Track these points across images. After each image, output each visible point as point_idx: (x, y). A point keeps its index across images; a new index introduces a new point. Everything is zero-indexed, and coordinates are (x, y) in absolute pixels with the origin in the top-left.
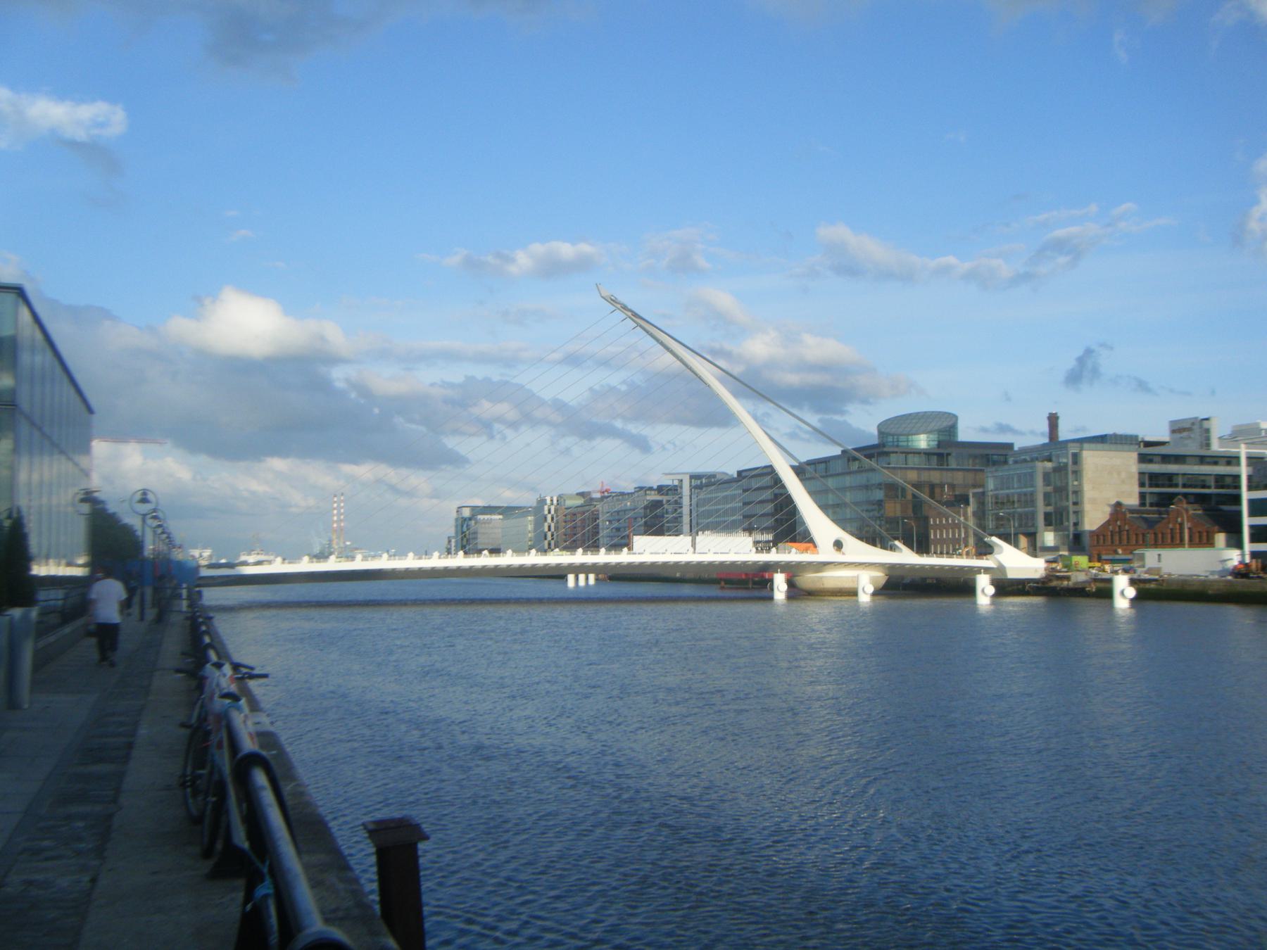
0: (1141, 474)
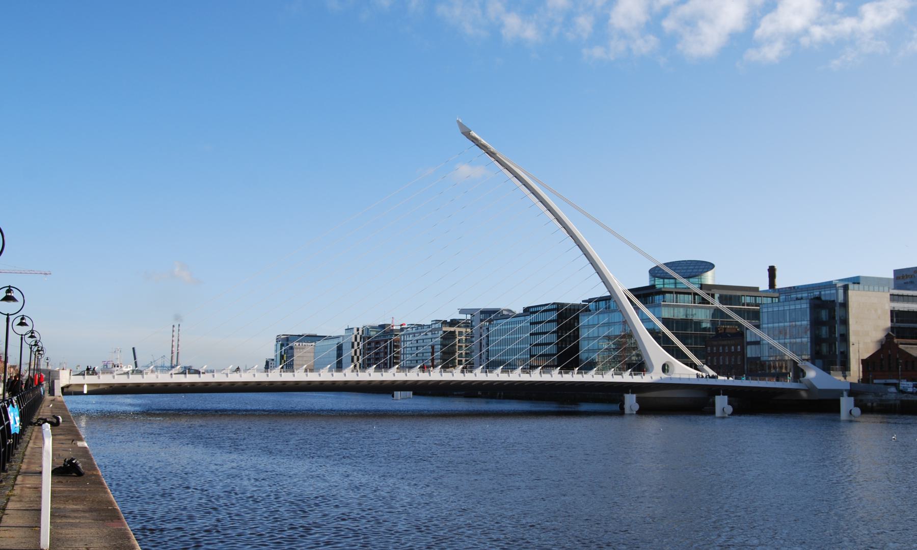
0: (892, 312)
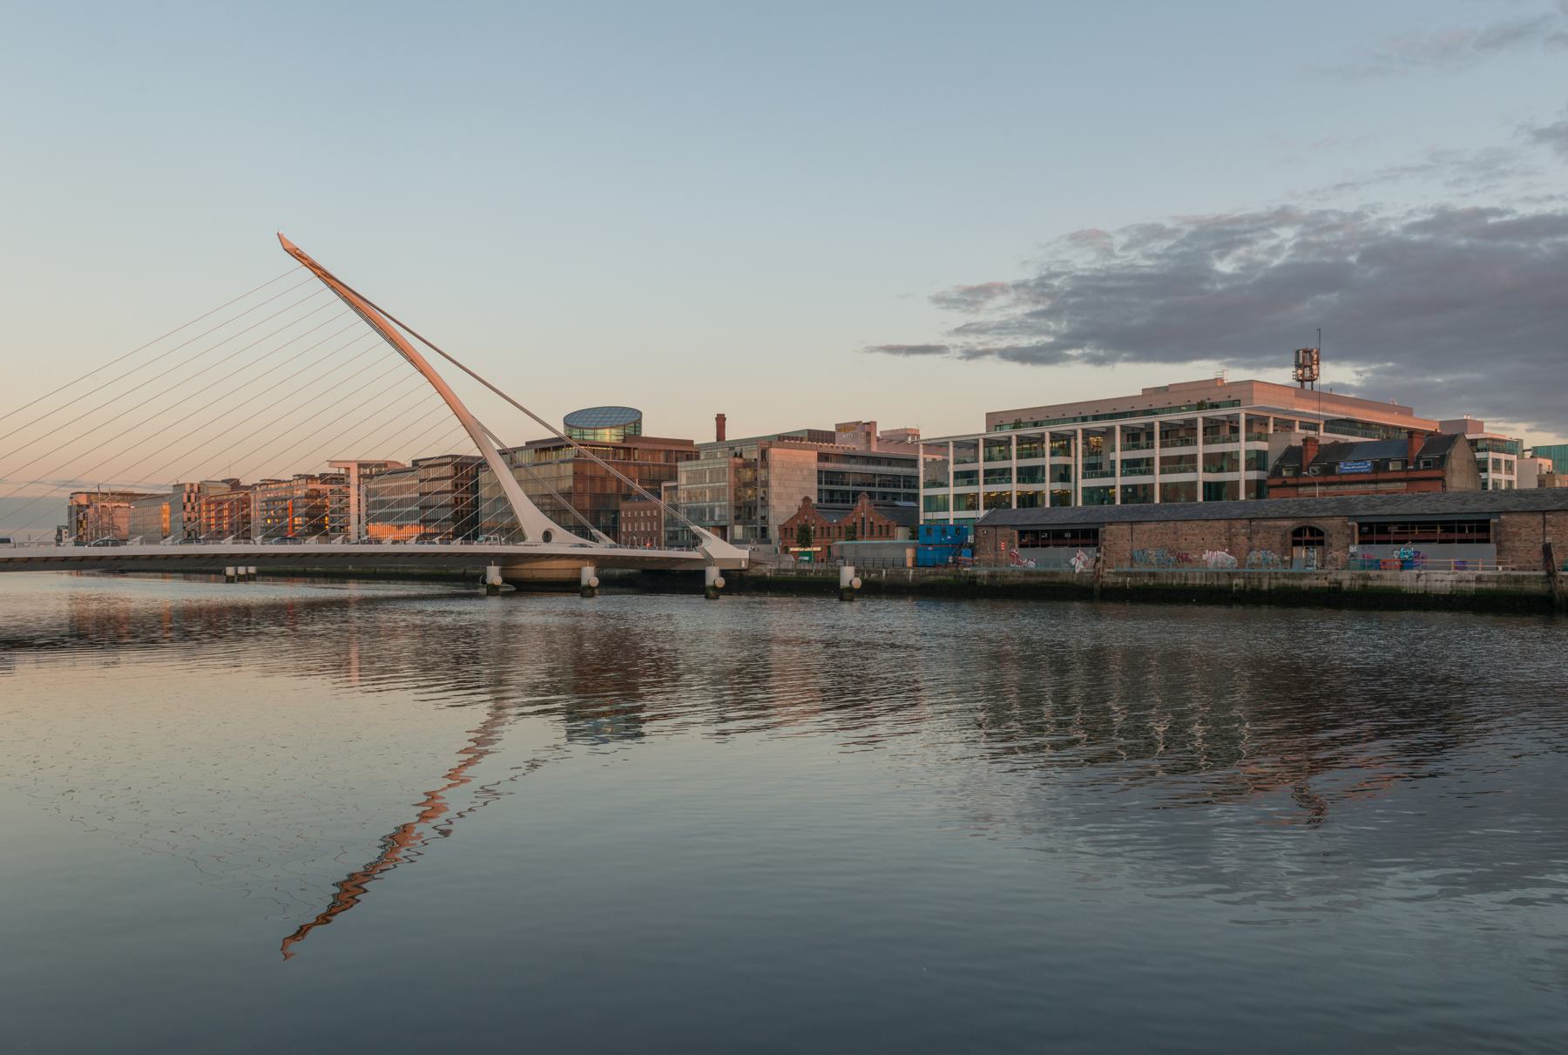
0: (820, 472)
